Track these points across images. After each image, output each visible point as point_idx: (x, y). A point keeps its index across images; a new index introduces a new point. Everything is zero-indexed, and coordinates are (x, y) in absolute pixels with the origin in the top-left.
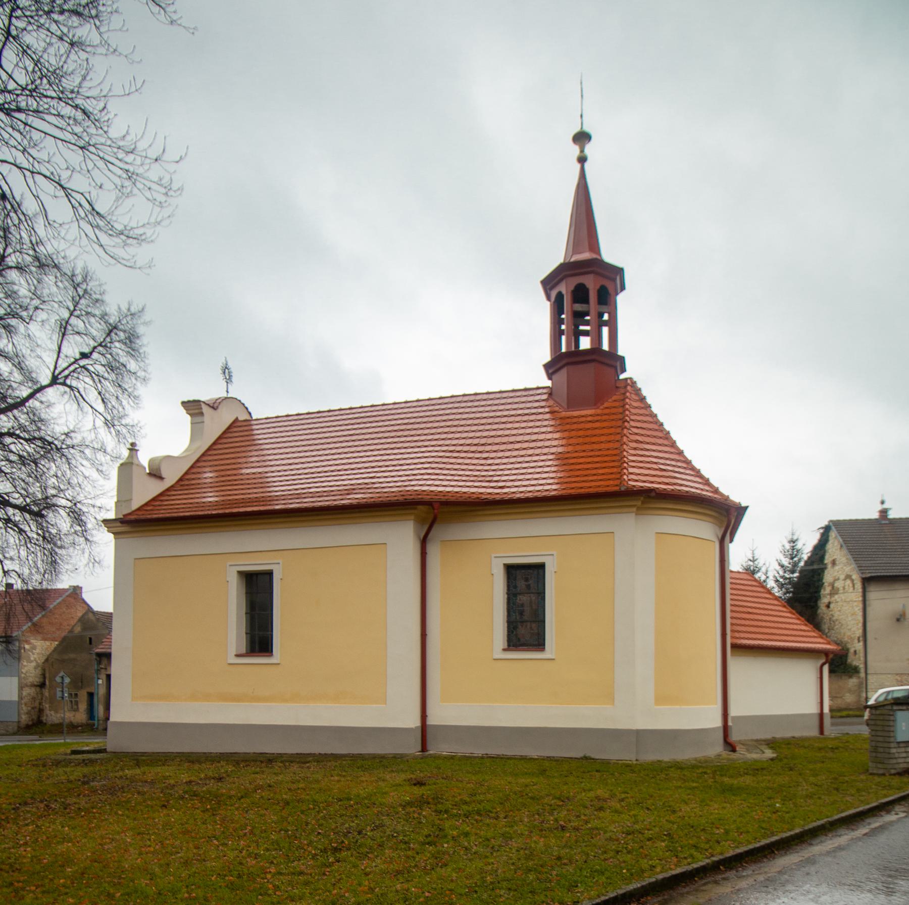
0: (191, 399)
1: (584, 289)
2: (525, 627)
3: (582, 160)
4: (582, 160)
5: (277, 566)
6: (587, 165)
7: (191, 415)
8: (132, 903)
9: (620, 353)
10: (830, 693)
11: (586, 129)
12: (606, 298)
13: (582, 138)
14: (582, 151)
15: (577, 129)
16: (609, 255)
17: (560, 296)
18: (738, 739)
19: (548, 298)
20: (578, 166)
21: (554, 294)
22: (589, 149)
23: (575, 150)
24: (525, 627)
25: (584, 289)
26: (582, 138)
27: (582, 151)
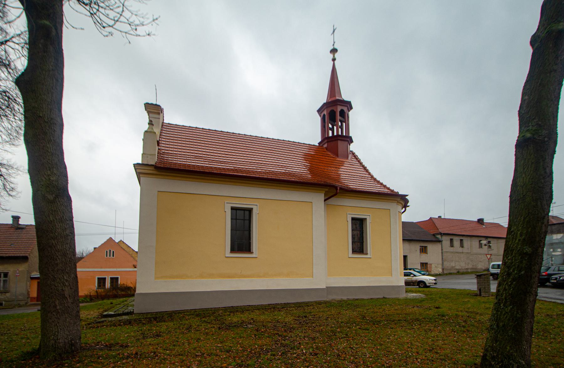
0: (150, 102)
1: (335, 111)
2: (241, 242)
3: (334, 60)
4: (334, 60)
5: (227, 256)
6: (335, 62)
7: (149, 113)
8: (515, 367)
9: (350, 135)
10: (105, 268)
11: (336, 47)
12: (344, 116)
13: (334, 51)
14: (334, 56)
15: (332, 48)
16: (345, 96)
17: (324, 115)
18: (167, 122)
19: (320, 116)
20: (332, 62)
21: (322, 115)
22: (337, 55)
23: (331, 56)
24: (241, 242)
25: (335, 111)
26: (334, 51)
27: (334, 56)
